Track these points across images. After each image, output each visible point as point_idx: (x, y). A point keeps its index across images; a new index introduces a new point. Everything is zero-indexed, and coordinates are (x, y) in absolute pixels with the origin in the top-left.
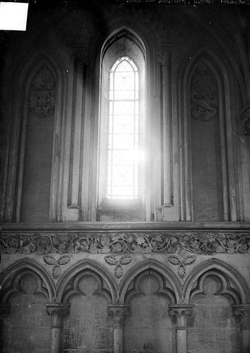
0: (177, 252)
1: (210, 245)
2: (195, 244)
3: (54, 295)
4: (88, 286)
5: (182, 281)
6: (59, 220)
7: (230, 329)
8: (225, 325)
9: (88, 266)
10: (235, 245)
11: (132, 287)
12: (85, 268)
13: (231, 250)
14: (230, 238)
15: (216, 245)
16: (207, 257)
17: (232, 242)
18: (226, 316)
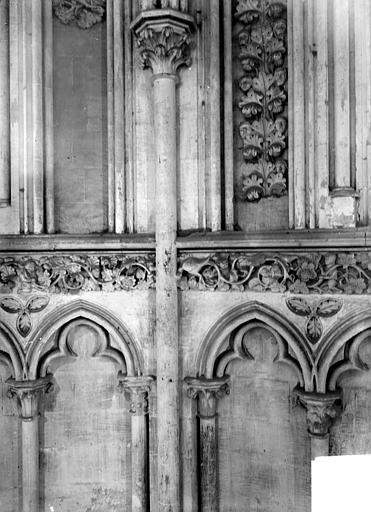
0: (15, 289)
1: (70, 277)
2: (45, 278)
3: (311, 367)
4: (84, 341)
5: (24, 341)
6: (26, 230)
7: (117, 411)
8: (108, 405)
9: (256, 316)
10: (113, 277)
11: (341, 357)
12: (253, 318)
13: (108, 286)
14: (107, 266)
15: (80, 279)
16: (67, 299)
17: (108, 273)
18: (111, 389)
